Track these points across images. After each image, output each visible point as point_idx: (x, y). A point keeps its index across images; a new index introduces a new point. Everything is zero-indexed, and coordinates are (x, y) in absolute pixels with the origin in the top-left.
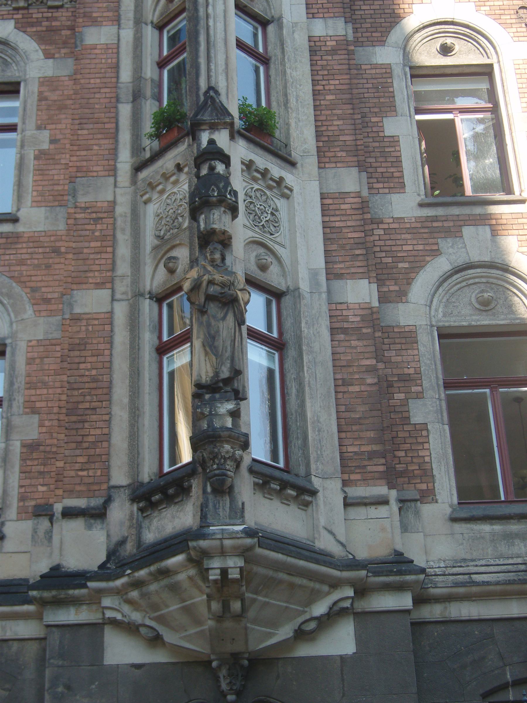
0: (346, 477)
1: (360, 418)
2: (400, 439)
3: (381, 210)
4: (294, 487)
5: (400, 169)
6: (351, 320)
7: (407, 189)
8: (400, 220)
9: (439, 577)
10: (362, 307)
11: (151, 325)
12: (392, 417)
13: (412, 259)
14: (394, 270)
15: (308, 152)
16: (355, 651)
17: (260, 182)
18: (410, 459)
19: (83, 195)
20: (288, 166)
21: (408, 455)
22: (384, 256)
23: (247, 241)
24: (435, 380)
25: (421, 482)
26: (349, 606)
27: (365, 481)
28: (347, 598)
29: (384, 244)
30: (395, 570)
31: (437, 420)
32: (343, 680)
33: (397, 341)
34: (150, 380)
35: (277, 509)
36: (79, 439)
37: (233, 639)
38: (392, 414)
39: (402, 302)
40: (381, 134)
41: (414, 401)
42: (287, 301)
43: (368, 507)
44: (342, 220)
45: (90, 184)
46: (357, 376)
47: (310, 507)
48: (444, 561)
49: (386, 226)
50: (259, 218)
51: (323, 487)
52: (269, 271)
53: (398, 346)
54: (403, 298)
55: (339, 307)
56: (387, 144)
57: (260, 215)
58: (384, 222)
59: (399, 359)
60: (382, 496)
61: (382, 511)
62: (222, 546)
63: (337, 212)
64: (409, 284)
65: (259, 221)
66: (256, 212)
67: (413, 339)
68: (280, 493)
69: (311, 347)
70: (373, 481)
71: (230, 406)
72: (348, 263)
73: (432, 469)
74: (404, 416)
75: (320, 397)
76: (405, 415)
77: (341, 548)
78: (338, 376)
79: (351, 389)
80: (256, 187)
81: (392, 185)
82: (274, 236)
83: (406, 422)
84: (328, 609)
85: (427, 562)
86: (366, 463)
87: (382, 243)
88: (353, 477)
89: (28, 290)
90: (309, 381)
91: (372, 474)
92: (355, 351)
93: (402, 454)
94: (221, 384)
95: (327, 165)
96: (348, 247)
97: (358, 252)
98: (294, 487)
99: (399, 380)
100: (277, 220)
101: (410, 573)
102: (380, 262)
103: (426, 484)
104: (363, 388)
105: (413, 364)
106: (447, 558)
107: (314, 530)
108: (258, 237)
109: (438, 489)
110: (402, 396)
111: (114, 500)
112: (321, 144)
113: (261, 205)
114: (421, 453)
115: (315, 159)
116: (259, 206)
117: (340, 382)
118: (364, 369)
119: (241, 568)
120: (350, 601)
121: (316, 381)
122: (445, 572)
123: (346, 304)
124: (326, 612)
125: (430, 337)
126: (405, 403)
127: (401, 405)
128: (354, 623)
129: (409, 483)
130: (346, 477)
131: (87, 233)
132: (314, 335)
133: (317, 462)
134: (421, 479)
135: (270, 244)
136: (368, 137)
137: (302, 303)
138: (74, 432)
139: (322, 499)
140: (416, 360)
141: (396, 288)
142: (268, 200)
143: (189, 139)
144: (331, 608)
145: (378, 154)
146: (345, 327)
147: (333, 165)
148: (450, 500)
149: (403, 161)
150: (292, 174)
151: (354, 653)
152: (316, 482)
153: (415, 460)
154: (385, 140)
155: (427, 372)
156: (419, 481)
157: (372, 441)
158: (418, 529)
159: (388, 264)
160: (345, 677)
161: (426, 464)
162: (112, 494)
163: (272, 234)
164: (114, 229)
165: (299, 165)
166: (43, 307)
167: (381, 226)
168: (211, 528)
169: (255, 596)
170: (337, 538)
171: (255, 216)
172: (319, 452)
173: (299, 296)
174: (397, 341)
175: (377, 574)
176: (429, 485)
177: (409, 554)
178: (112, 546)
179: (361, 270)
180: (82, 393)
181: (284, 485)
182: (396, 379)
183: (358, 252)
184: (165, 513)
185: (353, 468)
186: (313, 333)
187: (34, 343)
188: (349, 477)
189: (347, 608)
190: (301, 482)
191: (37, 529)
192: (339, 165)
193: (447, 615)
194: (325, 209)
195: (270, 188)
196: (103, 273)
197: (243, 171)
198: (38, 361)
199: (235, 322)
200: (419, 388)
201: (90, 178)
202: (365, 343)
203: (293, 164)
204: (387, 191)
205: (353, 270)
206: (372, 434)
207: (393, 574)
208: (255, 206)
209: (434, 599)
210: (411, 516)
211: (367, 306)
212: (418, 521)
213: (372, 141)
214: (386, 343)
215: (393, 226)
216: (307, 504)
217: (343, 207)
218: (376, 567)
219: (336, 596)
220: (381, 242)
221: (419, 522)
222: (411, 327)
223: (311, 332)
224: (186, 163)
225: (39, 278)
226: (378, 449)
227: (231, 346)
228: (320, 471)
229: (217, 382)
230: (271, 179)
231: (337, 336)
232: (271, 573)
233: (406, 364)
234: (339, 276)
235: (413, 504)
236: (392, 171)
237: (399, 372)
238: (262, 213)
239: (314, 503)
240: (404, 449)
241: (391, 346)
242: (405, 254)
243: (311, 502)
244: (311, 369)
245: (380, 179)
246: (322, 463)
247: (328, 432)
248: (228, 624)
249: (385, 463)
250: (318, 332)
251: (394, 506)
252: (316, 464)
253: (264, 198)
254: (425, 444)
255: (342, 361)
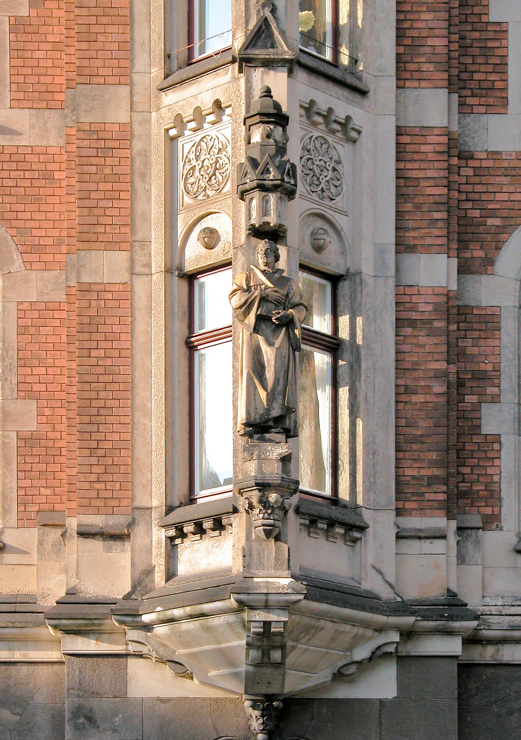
0: (400, 505)
1: (421, 436)
2: (466, 452)
3: (473, 138)
4: (342, 524)
5: (504, 77)
6: (421, 310)
7: (511, 107)
8: (494, 155)
9: (494, 617)
10: (436, 292)
11: (180, 312)
12: (460, 424)
13: (505, 213)
14: (481, 228)
15: (385, 71)
16: (396, 695)
17: (320, 127)
18: (475, 477)
19: (86, 111)
20: (357, 97)
21: (474, 472)
22: (471, 207)
23: (302, 216)
24: (517, 380)
25: (487, 506)
26: (393, 651)
27: (421, 510)
28: (393, 643)
29: (471, 190)
30: (446, 615)
31: (513, 432)
32: (381, 725)
33: (475, 326)
34: (179, 382)
35: (323, 548)
36: (94, 444)
37: (269, 683)
38: (460, 420)
39: (486, 274)
40: (484, 19)
41: (488, 405)
42: (344, 287)
43: (423, 541)
44: (421, 167)
45: (95, 96)
46: (422, 383)
47: (359, 543)
48: (502, 598)
49: (476, 164)
50: (318, 179)
51: (374, 520)
52: (325, 252)
53: (476, 334)
54: (489, 267)
55: (408, 291)
56: (491, 35)
57: (318, 176)
58: (475, 157)
59: (475, 350)
60: (439, 529)
61: (439, 545)
62: (267, 601)
63: (416, 157)
64: (498, 249)
65: (318, 183)
66: (314, 172)
67: (495, 324)
68: (328, 533)
69: (371, 350)
70: (430, 510)
71: (281, 450)
72: (423, 231)
73: (500, 490)
74: (474, 424)
75: (378, 413)
76: (475, 422)
77: (389, 589)
78: (401, 382)
79: (415, 398)
80: (316, 134)
81: (491, 101)
82: (334, 202)
83: (475, 432)
84: (371, 654)
85: (483, 597)
86: (424, 489)
87: (469, 188)
88: (409, 505)
89: (14, 232)
90: (366, 394)
91: (430, 503)
92: (422, 350)
93: (466, 470)
94: (271, 423)
95: (408, 84)
96: (426, 208)
97: (437, 216)
98: (342, 524)
99: (473, 378)
100: (339, 177)
101: (463, 619)
102: (464, 215)
103: (491, 508)
104: (429, 398)
105: (492, 359)
106: (506, 595)
107: (360, 570)
108: (316, 208)
109: (505, 515)
110: (474, 399)
111: (138, 523)
112: (402, 50)
113: (320, 160)
114: (490, 471)
115: (393, 81)
116: (318, 163)
117: (402, 390)
118: (431, 374)
119: (285, 623)
120: (395, 646)
121: (374, 391)
122: (501, 612)
123: (417, 287)
124: (369, 657)
125: (517, 324)
126: (476, 407)
127: (472, 410)
128: (397, 667)
129: (472, 506)
130: (400, 505)
131: (93, 169)
132: (376, 333)
133: (369, 491)
134: (486, 501)
135: (330, 214)
136: (467, 22)
137: (363, 293)
138: (87, 436)
139: (372, 534)
140: (496, 353)
141: (481, 254)
142: (329, 150)
143: (233, 68)
144: (373, 653)
145: (477, 51)
146: (413, 318)
147: (416, 84)
148: (517, 527)
149: (509, 63)
150: (362, 107)
151: (394, 698)
152: (367, 516)
153: (481, 479)
154: (489, 29)
155: (507, 369)
156: (484, 504)
157: (433, 464)
158: (476, 561)
159: (475, 220)
160: (383, 721)
161: (494, 485)
162: (136, 516)
163: (332, 199)
164: (132, 173)
165: (371, 94)
166: (35, 257)
167: (471, 163)
168: (255, 580)
169: (296, 644)
170: (386, 578)
171: (313, 176)
172: (372, 480)
173: (361, 284)
174: (475, 326)
175: (425, 618)
176: (495, 509)
177: (464, 597)
178: (137, 576)
179: (440, 241)
180: (95, 387)
181: (332, 523)
182: (469, 376)
183: (437, 216)
184: (199, 546)
185: (409, 495)
186: (375, 331)
187: (26, 306)
188: (404, 505)
189: (391, 653)
190: (350, 518)
191: (43, 540)
192: (423, 84)
193: (499, 657)
194: (400, 150)
195: (333, 132)
196: (116, 229)
197: (301, 116)
198: (32, 330)
199: (289, 348)
200: (496, 389)
201: (96, 86)
202: (435, 340)
203: (363, 93)
204: (483, 109)
205: (428, 241)
206: (434, 456)
207: (444, 619)
208: (313, 163)
209: (486, 641)
210: (470, 546)
211: (441, 291)
212: (477, 551)
213: (470, 29)
214: (461, 328)
215: (485, 164)
216: (355, 541)
217: (424, 148)
218: (425, 610)
219: (380, 640)
220: (469, 186)
221: (479, 552)
222: (494, 309)
223: (373, 329)
224: (229, 104)
225: (28, 216)
226: (439, 474)
227: (284, 378)
228: (372, 501)
229: (268, 420)
230: (336, 121)
231: (403, 329)
232: (313, 622)
233: (483, 358)
234: (412, 249)
235: (474, 532)
236: (492, 79)
237: (474, 367)
238: (322, 171)
239: (363, 539)
240: (470, 465)
241: (468, 332)
242: (498, 207)
243: (360, 539)
244: (369, 378)
245: (475, 91)
246: (375, 493)
247: (384, 456)
248: (267, 671)
249: (446, 491)
250: (380, 330)
251: (452, 538)
252: (368, 494)
253: (325, 146)
254: (495, 460)
255: (406, 363)
